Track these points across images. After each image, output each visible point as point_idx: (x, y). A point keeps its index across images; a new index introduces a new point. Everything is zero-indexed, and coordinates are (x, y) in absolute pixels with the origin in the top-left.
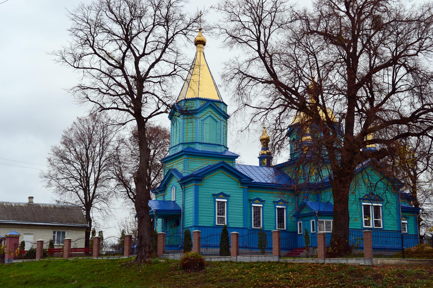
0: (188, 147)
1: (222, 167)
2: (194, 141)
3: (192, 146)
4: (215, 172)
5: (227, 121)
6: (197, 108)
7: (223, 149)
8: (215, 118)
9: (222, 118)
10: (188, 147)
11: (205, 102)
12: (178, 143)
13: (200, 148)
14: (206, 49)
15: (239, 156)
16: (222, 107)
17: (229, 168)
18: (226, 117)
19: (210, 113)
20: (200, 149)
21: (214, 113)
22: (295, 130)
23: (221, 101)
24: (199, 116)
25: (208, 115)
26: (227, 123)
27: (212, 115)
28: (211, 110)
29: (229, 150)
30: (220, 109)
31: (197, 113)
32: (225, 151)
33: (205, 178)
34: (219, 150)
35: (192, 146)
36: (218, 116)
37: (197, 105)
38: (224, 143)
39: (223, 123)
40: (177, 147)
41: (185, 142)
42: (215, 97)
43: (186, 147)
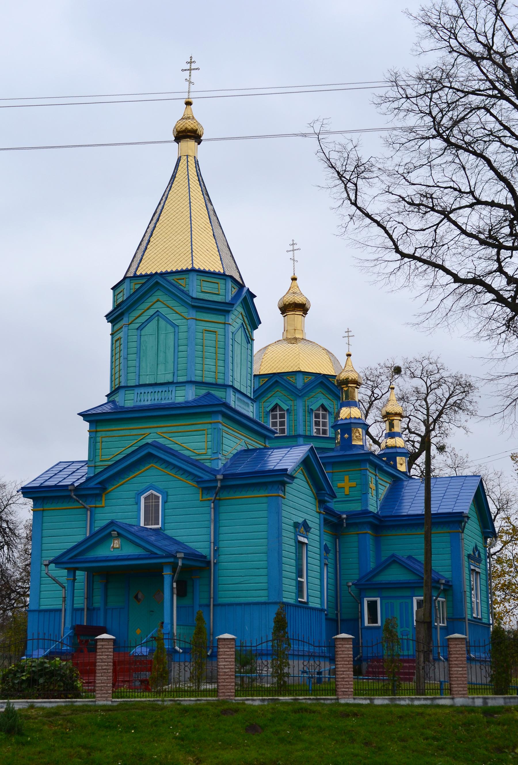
20: (129, 404)
35: (218, 393)
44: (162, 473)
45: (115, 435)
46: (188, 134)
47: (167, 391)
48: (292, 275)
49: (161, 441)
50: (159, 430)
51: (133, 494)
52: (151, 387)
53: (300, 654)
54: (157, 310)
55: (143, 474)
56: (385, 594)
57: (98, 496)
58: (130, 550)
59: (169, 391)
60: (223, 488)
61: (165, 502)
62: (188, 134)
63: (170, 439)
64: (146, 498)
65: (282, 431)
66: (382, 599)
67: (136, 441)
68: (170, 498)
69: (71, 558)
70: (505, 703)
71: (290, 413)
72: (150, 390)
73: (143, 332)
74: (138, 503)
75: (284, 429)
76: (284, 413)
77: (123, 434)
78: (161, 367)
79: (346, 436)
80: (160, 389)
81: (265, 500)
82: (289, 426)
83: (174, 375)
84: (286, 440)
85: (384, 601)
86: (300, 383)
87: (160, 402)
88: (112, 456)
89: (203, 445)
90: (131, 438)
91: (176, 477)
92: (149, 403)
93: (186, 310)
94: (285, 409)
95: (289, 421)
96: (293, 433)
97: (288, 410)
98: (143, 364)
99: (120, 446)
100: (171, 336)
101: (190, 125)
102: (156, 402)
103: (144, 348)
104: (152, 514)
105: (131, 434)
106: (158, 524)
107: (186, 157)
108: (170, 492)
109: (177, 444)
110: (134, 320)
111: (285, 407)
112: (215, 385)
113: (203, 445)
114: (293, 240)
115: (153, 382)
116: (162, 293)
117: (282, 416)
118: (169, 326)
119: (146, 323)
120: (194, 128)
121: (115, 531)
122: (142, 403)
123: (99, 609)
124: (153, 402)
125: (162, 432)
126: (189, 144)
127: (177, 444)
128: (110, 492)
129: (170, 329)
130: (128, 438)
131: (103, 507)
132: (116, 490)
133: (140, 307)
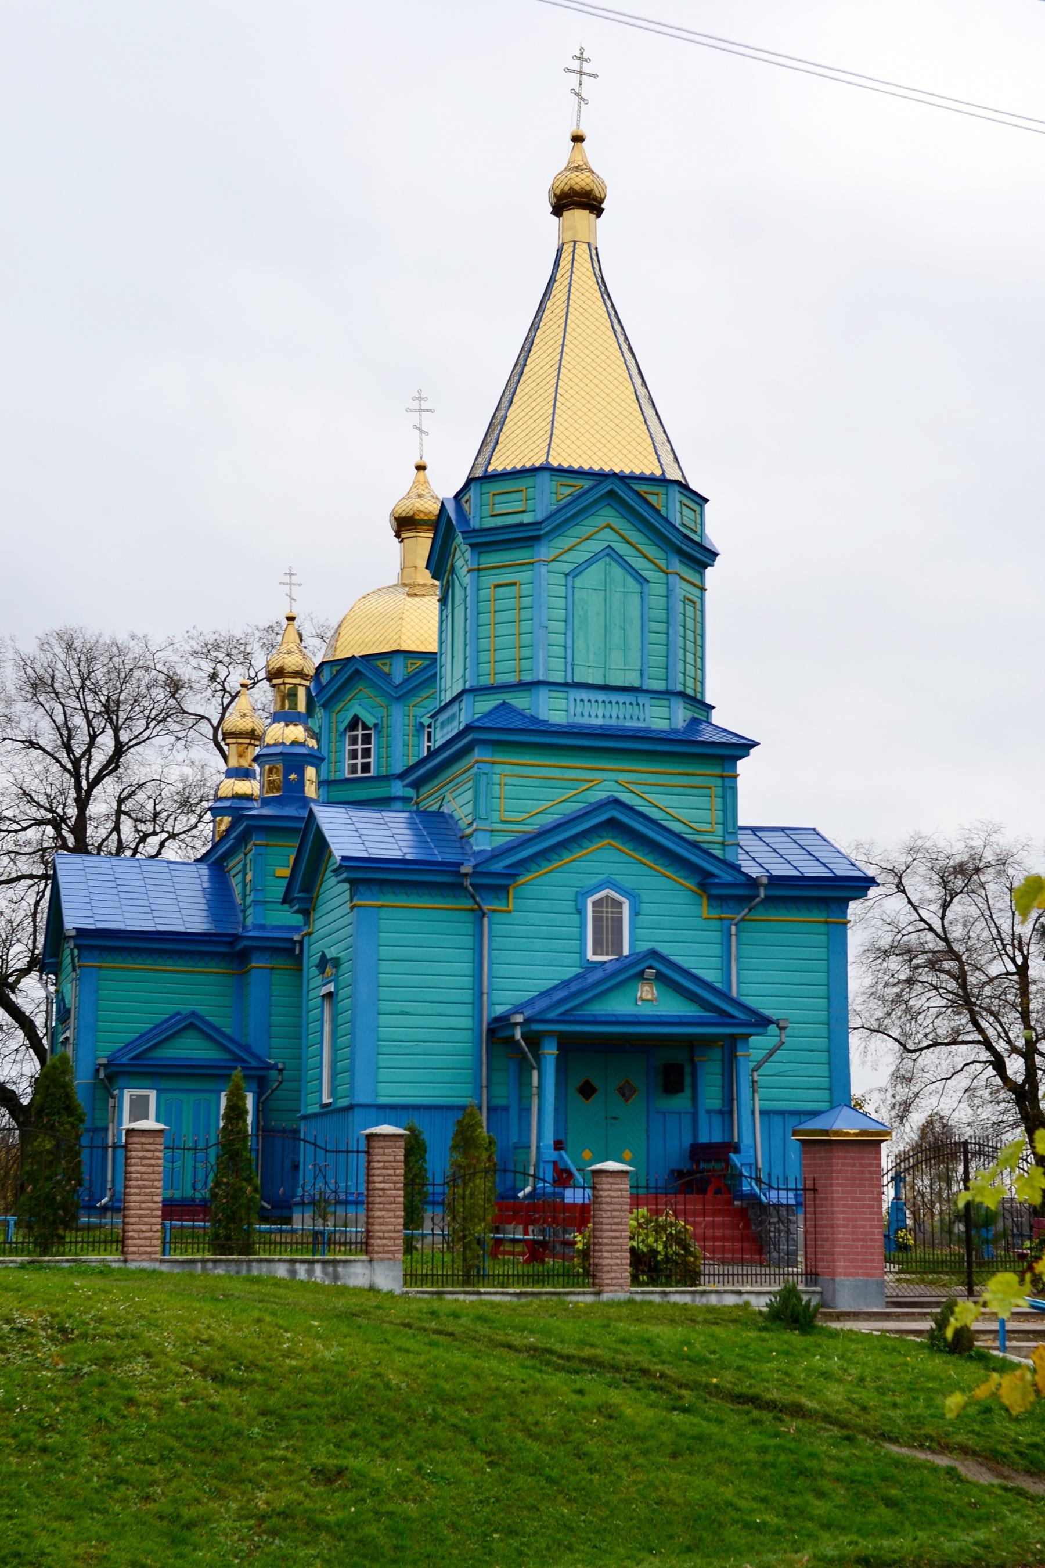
0: (504, 703)
1: (613, 826)
2: (527, 678)
3: (520, 701)
4: (586, 843)
5: (702, 575)
6: (539, 518)
7: (680, 715)
8: (638, 562)
9: (677, 565)
10: (504, 703)
11: (587, 484)
12: (458, 689)
13: (553, 709)
14: (605, 229)
15: (756, 744)
16: (677, 513)
17: (651, 834)
18: (700, 557)
19: (608, 534)
20: (557, 718)
21: (635, 536)
22: (41, 971)
23: (673, 474)
24: (545, 551)
25: (595, 546)
26: (703, 589)
27: (621, 548)
28: (619, 523)
29: (716, 718)
30: (666, 520)
31: (538, 538)
32: (695, 722)
33: (522, 880)
34: (662, 718)
35: (520, 701)
36: (651, 551)
37: (536, 504)
38: (690, 682)
39: (682, 590)
40: (455, 708)
41: (485, 681)
42: (634, 459)
43: (485, 705)
44: (627, 859)
45: (532, 775)
46: (577, 200)
47: (635, 703)
48: (417, 460)
49: (626, 797)
50: (622, 777)
51: (570, 893)
52: (602, 692)
53: (350, 1198)
54: (608, 543)
55: (589, 857)
56: (165, 1084)
57: (501, 890)
58: (672, 1006)
59: (638, 704)
60: (768, 899)
61: (635, 913)
62: (577, 200)
63: (644, 796)
64: (595, 904)
65: (366, 768)
66: (159, 1091)
67: (575, 792)
68: (645, 908)
69: (562, 1014)
70: (693, 1301)
71: (380, 732)
72: (601, 696)
73: (579, 581)
74: (580, 912)
75: (369, 763)
76: (370, 735)
77: (549, 776)
78: (616, 656)
79: (293, 776)
80: (615, 697)
81: (823, 928)
82: (379, 757)
83: (641, 675)
84: (376, 784)
85: (165, 1096)
86: (399, 671)
87: (622, 723)
88: (527, 815)
89: (705, 815)
90: (565, 784)
91: (655, 870)
92: (599, 721)
93: (663, 555)
94: (371, 725)
95: (379, 747)
96: (383, 772)
97: (376, 725)
98: (580, 644)
99: (542, 797)
100: (636, 599)
101: (580, 181)
102: (613, 722)
103: (581, 613)
104: (607, 934)
105: (566, 776)
106: (595, 953)
107: (572, 244)
108: (645, 895)
109: (656, 807)
110: (561, 554)
111: (370, 720)
112: (521, 686)
113: (705, 815)
114: (420, 391)
115: (601, 682)
116: (614, 513)
117: (367, 739)
118: (630, 581)
119: (585, 565)
120: (588, 189)
121: (650, 967)
122: (585, 721)
123: (506, 1109)
124: (608, 722)
125: (630, 780)
126: (578, 216)
127: (656, 807)
128: (522, 884)
129: (632, 584)
130: (559, 783)
131: (509, 912)
132: (534, 882)
133: (570, 532)
